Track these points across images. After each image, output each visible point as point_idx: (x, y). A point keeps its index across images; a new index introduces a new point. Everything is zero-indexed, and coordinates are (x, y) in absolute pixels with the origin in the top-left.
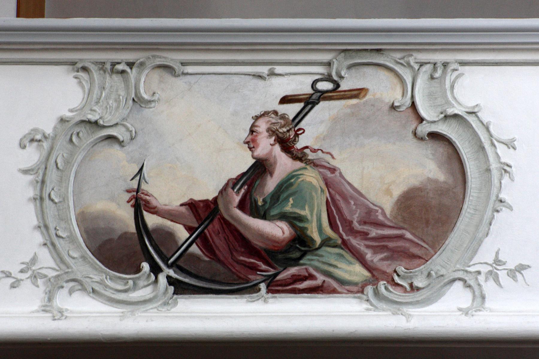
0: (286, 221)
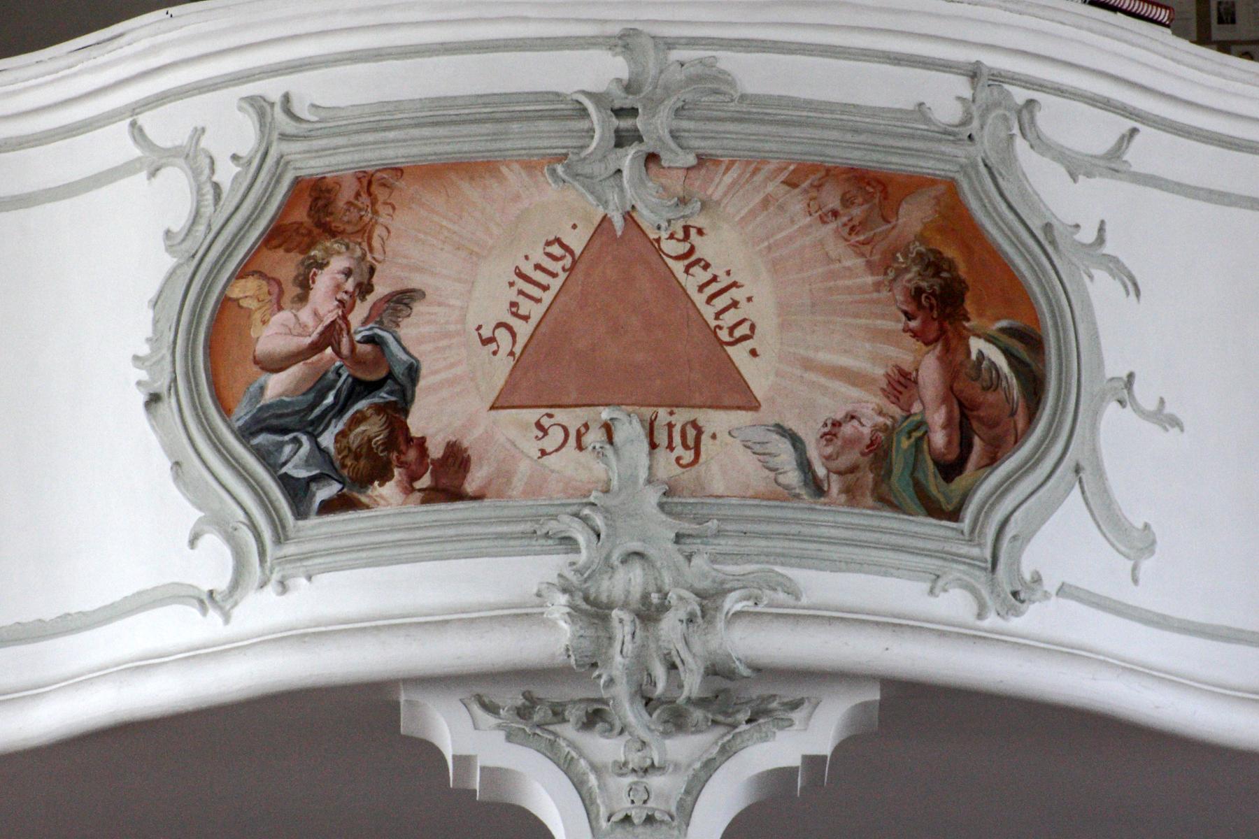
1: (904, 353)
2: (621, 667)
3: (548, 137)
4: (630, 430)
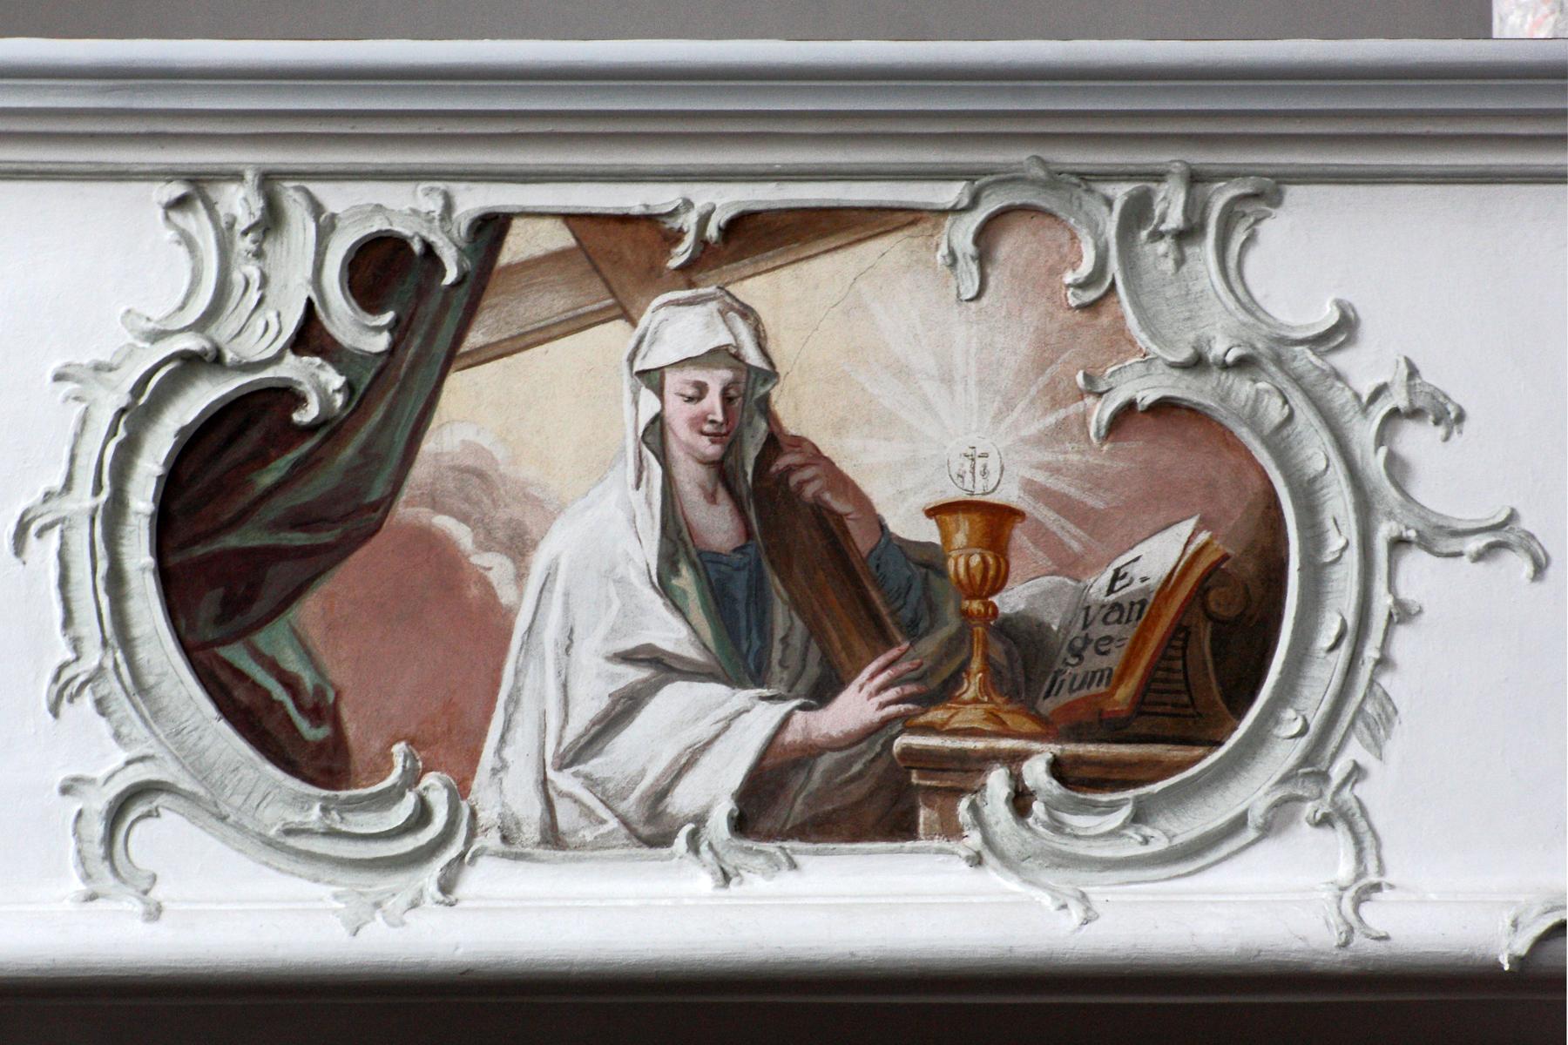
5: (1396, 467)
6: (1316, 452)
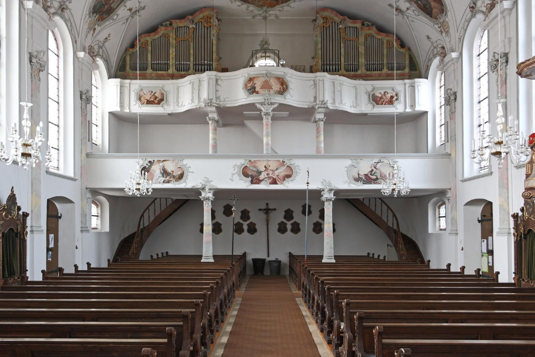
0: (221, 227)
1: (280, 87)
2: (502, 140)
3: (263, 75)
4: (267, 90)
5: (188, 169)
6: (185, 169)
